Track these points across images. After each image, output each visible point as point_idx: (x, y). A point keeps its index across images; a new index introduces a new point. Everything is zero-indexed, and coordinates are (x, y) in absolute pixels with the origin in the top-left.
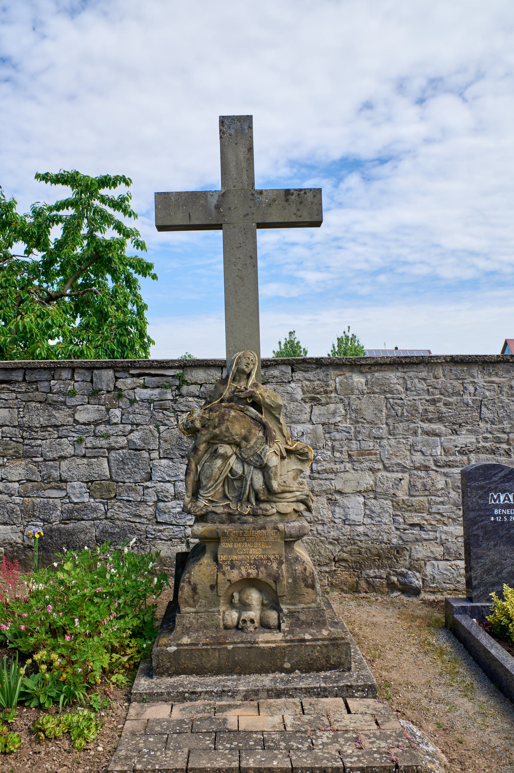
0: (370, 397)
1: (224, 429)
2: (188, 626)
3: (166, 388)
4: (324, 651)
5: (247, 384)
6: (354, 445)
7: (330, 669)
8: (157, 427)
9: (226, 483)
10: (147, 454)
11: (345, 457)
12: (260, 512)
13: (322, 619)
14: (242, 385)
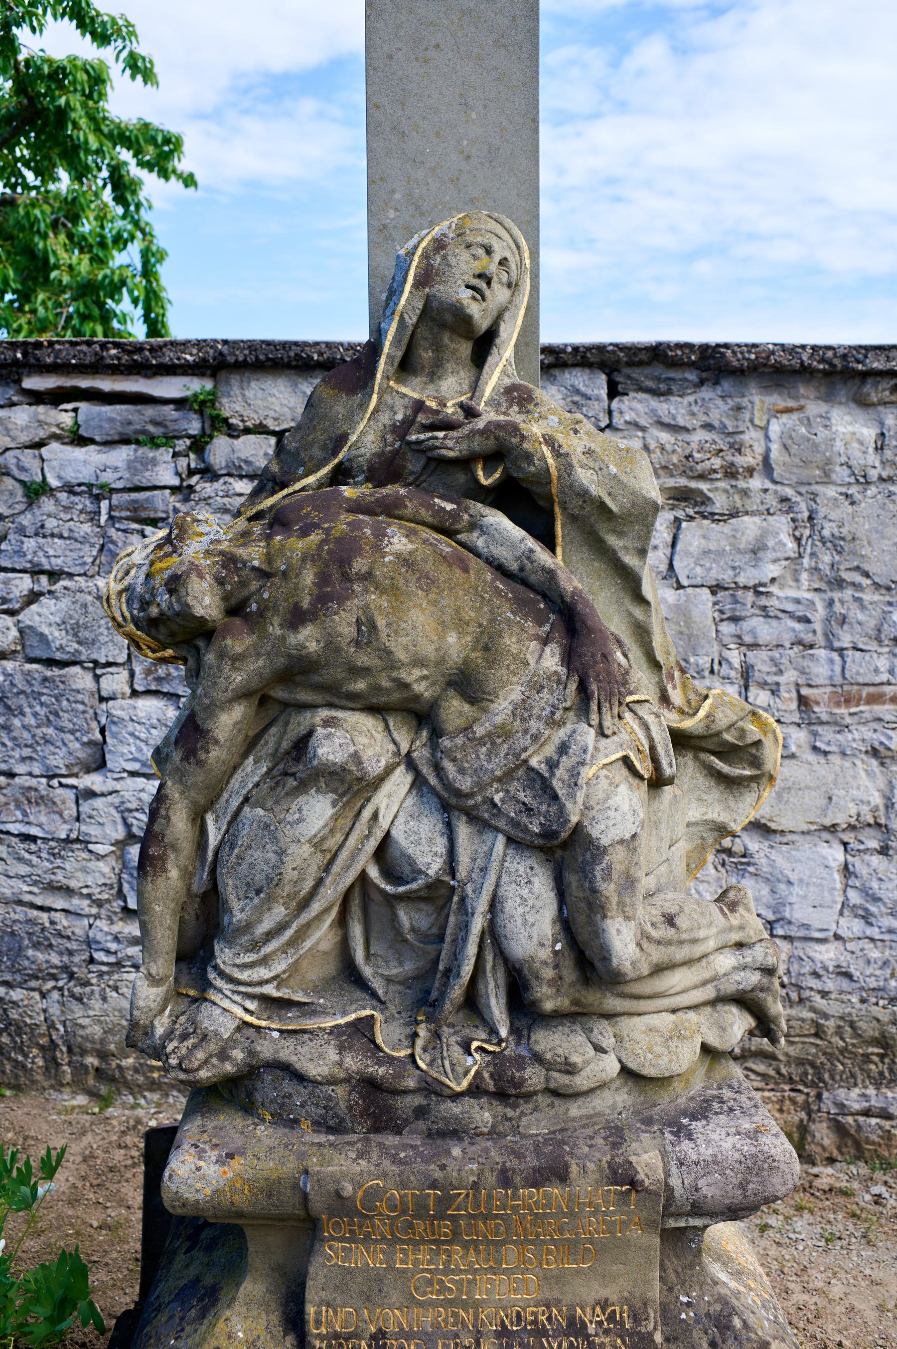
3: (153, 442)
5: (475, 387)
6: (823, 665)
10: (89, 677)
12: (534, 1076)
14: (449, 391)
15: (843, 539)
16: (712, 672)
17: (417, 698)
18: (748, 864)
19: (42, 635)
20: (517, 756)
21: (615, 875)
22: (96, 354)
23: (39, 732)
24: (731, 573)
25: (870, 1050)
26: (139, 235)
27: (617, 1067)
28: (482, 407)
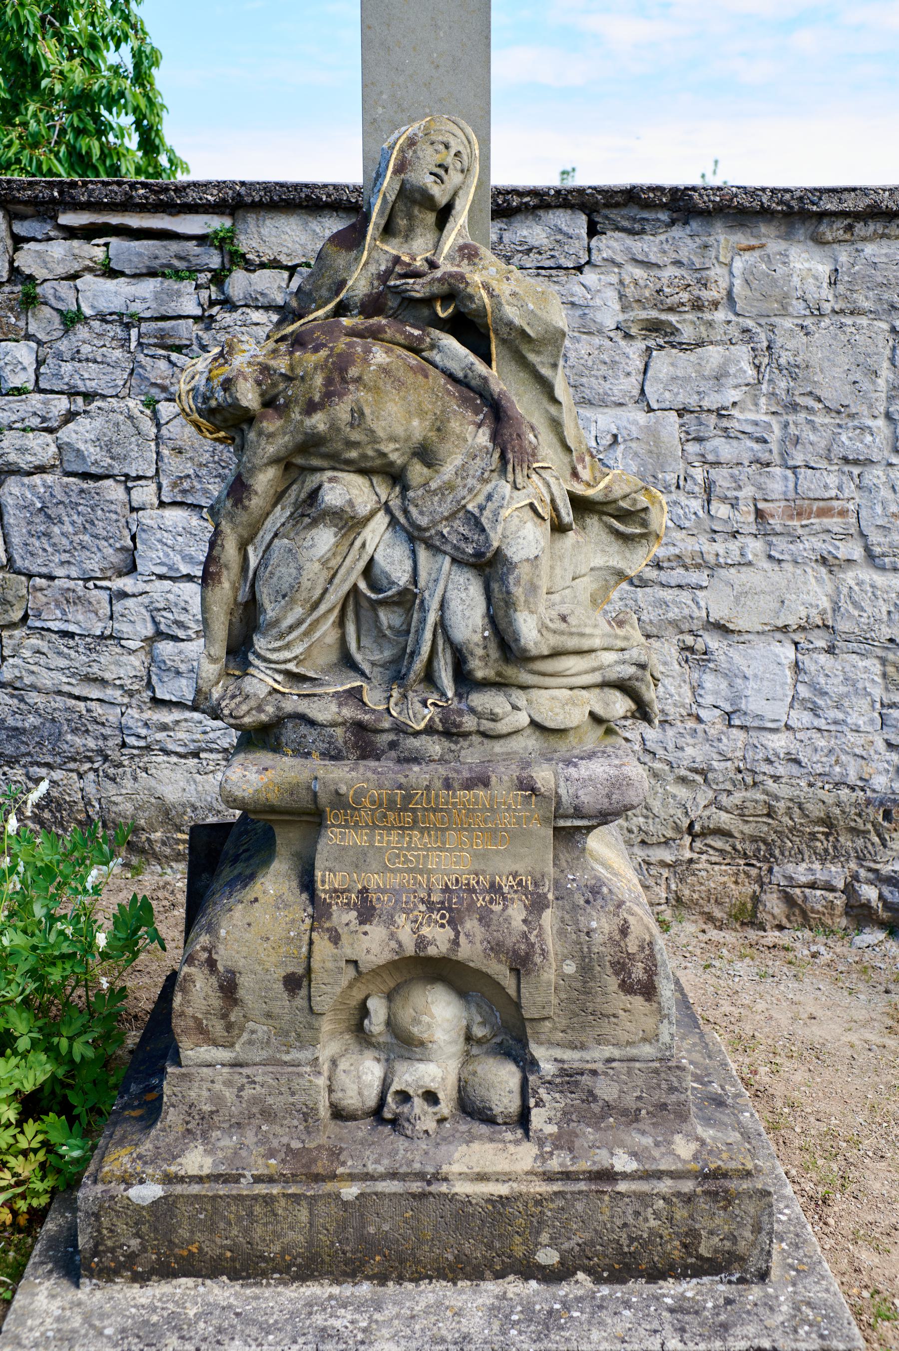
0: (842, 326)
1: (345, 417)
2: (207, 1108)
3: (177, 275)
4: (681, 1213)
5: (437, 246)
6: (778, 483)
7: (698, 1272)
8: (152, 404)
9: (350, 615)
10: (121, 489)
11: (746, 518)
12: (469, 723)
13: (673, 1098)
14: (417, 249)
15: (798, 367)
16: (678, 487)
17: (392, 464)
18: (709, 661)
19: (78, 450)
20: (458, 502)
21: (523, 582)
22: (126, 193)
23: (76, 539)
24: (696, 397)
25: (817, 829)
26: (131, 33)
27: (528, 720)
28: (441, 261)
